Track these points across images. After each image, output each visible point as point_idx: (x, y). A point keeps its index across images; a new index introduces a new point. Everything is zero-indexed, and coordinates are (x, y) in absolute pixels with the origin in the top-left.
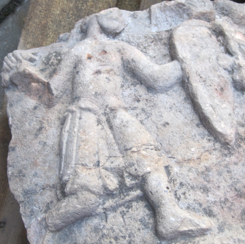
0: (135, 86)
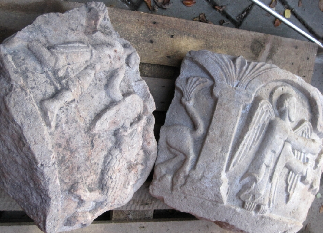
0: (106, 78)
